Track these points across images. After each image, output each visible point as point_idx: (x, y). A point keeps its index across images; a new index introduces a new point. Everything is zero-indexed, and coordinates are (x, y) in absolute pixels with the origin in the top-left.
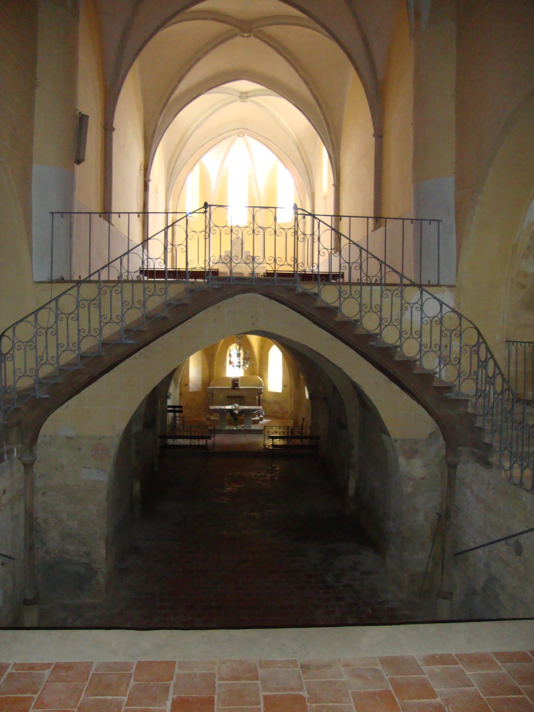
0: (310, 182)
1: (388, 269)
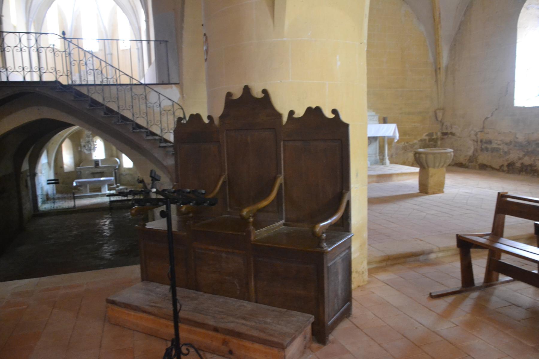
0: (134, 12)
1: (121, 73)
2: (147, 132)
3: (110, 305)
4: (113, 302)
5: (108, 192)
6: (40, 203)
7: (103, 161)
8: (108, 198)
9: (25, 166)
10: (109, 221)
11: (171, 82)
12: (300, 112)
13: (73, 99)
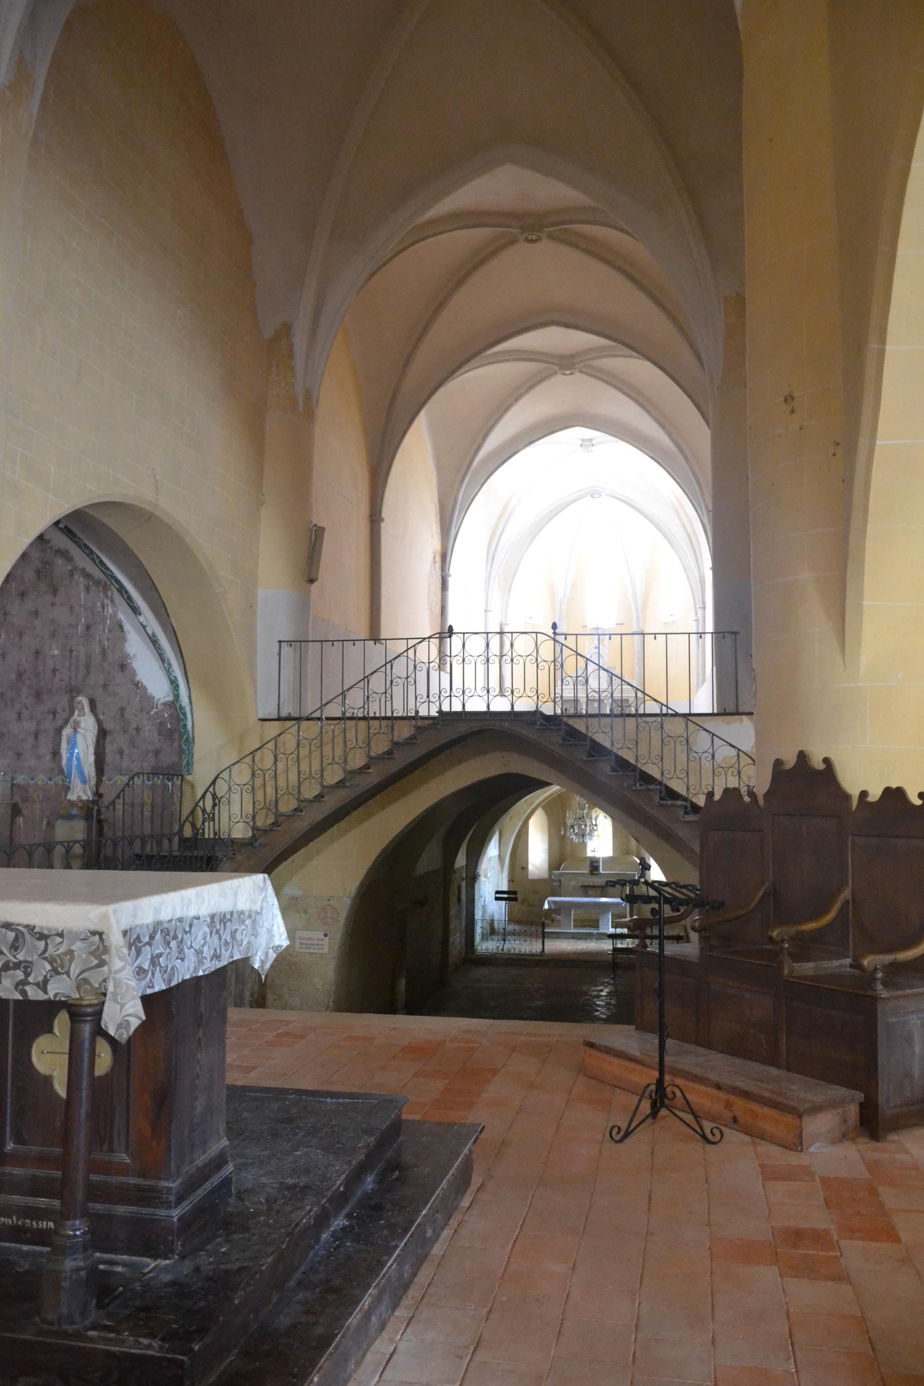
0: (697, 561)
2: (686, 807)
3: (588, 1049)
4: (591, 1045)
5: (612, 931)
6: (478, 938)
7: (607, 861)
8: (610, 941)
9: (461, 860)
10: (607, 990)
11: (740, 711)
12: (875, 794)
13: (560, 742)
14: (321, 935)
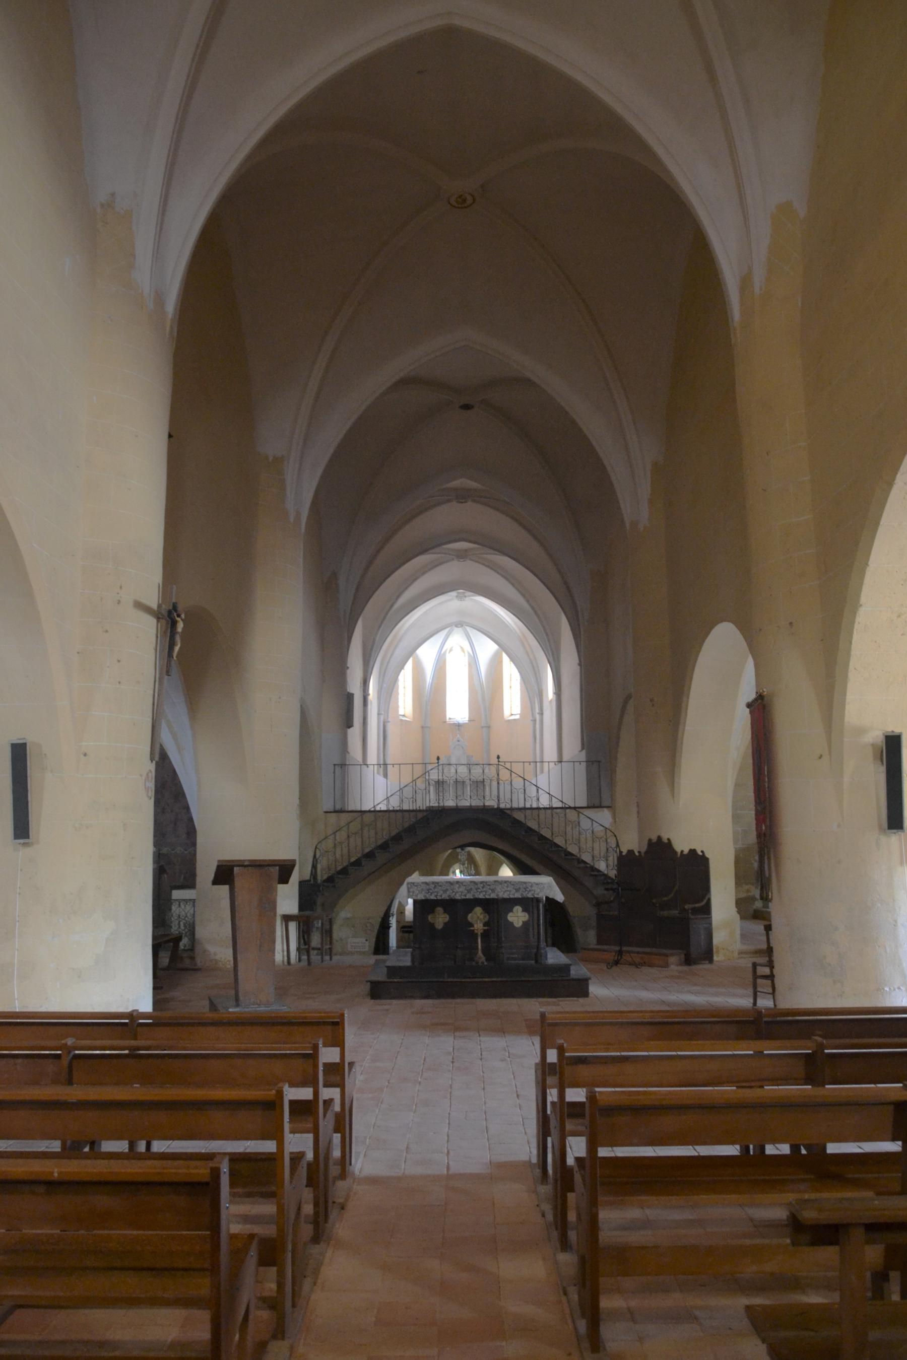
0: (535, 674)
11: (603, 804)
12: (686, 851)
14: (364, 940)
